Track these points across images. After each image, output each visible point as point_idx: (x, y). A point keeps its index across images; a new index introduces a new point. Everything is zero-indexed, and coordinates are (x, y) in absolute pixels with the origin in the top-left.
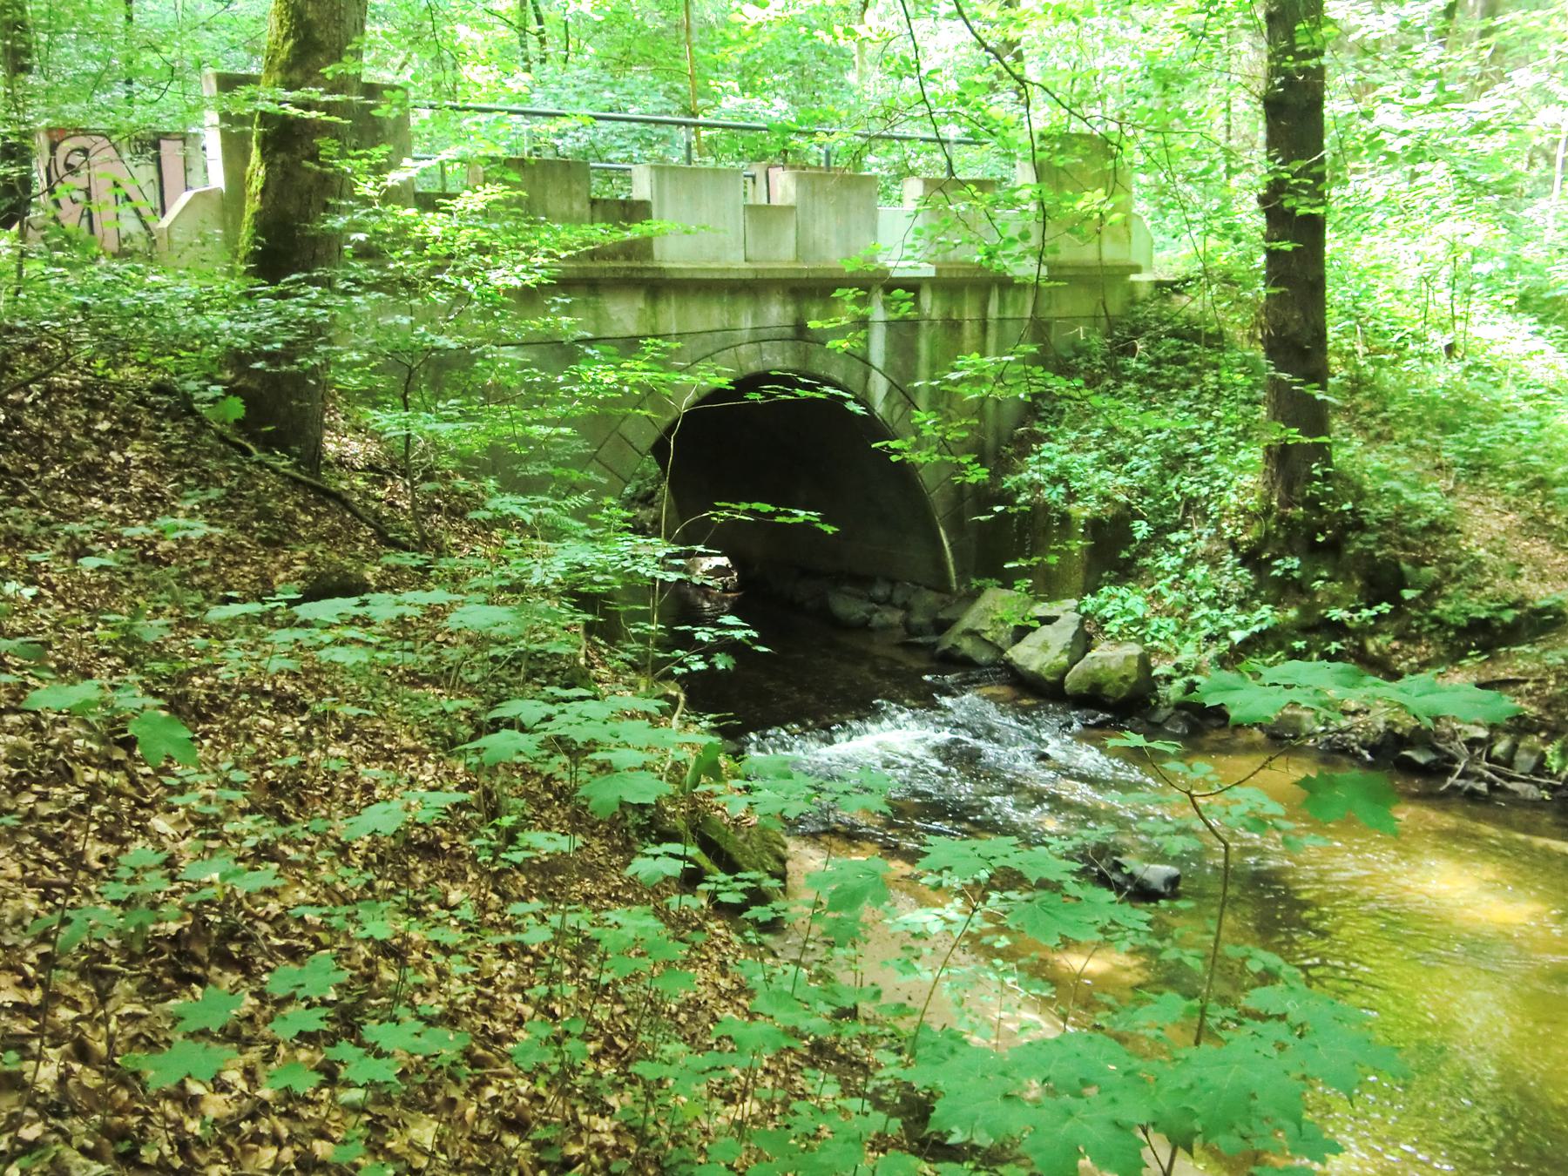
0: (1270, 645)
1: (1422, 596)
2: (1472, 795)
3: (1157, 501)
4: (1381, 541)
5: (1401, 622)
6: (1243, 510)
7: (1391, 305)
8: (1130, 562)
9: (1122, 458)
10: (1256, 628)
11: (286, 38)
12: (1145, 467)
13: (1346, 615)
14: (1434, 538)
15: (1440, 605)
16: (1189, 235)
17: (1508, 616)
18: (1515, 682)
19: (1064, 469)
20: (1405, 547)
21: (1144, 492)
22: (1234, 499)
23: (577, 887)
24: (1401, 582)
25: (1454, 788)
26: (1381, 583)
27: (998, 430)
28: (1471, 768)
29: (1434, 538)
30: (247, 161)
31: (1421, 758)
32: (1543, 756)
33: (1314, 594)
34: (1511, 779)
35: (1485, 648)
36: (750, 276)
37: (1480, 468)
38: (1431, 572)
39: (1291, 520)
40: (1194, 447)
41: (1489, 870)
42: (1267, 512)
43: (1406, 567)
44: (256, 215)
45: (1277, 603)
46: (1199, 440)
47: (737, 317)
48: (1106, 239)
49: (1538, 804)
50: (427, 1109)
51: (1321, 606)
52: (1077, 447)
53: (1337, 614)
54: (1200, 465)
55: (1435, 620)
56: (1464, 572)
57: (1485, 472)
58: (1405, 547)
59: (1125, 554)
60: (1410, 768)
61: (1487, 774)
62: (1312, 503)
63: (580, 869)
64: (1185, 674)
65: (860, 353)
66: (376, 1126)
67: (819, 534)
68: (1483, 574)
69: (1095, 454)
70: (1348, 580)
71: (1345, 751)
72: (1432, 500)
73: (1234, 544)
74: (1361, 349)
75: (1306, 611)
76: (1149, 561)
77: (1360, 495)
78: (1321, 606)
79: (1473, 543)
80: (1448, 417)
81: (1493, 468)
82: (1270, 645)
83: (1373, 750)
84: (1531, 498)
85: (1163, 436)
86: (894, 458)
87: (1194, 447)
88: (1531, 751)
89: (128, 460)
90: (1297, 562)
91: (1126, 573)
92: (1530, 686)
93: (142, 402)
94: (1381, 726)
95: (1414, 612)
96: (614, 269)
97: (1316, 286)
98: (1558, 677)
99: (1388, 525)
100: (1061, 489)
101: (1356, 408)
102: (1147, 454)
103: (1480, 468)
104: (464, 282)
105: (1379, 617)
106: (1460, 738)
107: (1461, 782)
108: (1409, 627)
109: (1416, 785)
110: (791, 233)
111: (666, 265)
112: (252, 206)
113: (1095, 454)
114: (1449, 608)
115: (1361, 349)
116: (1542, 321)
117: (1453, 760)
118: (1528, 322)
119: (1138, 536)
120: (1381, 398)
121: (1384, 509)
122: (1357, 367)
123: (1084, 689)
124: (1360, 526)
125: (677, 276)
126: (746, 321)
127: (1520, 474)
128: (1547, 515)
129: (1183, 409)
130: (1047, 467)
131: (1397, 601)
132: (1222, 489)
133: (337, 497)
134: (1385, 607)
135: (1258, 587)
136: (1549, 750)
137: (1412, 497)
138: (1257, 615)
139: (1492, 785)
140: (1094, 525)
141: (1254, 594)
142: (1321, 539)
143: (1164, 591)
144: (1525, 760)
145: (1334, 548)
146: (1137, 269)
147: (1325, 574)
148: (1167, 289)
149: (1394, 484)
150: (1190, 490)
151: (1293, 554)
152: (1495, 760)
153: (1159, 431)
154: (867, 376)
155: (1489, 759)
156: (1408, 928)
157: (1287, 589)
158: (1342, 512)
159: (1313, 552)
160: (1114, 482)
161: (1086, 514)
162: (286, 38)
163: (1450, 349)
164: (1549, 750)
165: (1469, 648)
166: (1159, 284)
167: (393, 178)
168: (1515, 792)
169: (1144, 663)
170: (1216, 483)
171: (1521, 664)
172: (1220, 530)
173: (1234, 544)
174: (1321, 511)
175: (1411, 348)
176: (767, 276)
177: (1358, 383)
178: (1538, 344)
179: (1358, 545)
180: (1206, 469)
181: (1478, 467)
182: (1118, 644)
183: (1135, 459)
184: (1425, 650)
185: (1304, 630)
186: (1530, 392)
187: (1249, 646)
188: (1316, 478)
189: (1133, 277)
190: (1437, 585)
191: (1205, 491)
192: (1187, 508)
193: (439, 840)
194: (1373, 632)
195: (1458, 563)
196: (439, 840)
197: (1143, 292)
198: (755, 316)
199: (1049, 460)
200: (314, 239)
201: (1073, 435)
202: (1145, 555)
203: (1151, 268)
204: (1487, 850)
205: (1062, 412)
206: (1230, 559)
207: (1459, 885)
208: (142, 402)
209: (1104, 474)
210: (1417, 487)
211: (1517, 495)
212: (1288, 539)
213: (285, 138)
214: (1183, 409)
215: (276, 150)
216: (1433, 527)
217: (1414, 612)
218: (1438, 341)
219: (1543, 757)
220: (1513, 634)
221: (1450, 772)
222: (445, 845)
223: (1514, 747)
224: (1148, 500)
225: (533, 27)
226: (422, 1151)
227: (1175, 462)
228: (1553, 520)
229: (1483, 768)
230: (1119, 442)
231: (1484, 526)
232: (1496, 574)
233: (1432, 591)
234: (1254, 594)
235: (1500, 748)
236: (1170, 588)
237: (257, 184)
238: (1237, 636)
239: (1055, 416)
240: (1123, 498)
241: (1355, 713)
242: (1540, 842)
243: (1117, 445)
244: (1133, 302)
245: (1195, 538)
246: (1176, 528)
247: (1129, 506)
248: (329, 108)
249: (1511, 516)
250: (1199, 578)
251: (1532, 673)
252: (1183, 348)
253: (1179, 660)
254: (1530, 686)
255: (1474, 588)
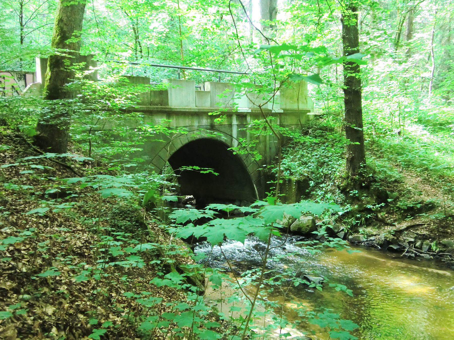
0: (350, 216)
1: (394, 201)
2: (410, 257)
3: (316, 175)
4: (381, 185)
5: (388, 209)
6: (341, 177)
7: (382, 121)
8: (309, 193)
9: (306, 163)
10: (346, 211)
11: (58, 35)
12: (313, 166)
13: (372, 207)
14: (396, 184)
15: (399, 203)
16: (323, 101)
17: (419, 206)
18: (422, 225)
19: (289, 166)
20: (388, 187)
21: (312, 173)
22: (338, 174)
23: (136, 280)
24: (387, 197)
25: (405, 256)
26: (381, 197)
27: (270, 157)
28: (409, 250)
29: (396, 184)
30: (46, 70)
31: (395, 247)
32: (431, 246)
33: (363, 201)
34: (421, 253)
35: (412, 215)
36: (197, 111)
37: (409, 165)
38: (396, 194)
39: (355, 179)
40: (326, 160)
41: (416, 277)
42: (348, 177)
43: (389, 193)
44: (48, 86)
45: (351, 204)
46: (328, 157)
47: (193, 122)
48: (300, 102)
49: (430, 260)
50: (51, 304)
51: (364, 204)
52: (293, 160)
53: (369, 206)
54: (328, 165)
55: (398, 207)
56: (405, 194)
57: (411, 166)
58: (388, 187)
59: (307, 191)
60: (392, 250)
61: (414, 251)
62: (360, 174)
63: (137, 275)
64: (326, 225)
65: (229, 134)
66: (31, 306)
67: (212, 172)
68: (411, 194)
69: (298, 162)
70: (372, 197)
71: (373, 246)
72: (395, 174)
73: (339, 187)
74: (374, 133)
75: (360, 206)
76: (314, 192)
77: (375, 172)
78: (364, 204)
79: (408, 186)
80: (400, 151)
81: (412, 165)
82: (350, 216)
83: (381, 245)
84: (424, 173)
85: (317, 157)
86: (234, 153)
87: (326, 160)
88: (427, 245)
89: (6, 155)
90: (357, 192)
91: (308, 196)
92: (426, 226)
93: (12, 140)
94: (383, 239)
95: (392, 205)
96: (157, 108)
97: (359, 113)
98: (434, 223)
99: (383, 181)
100: (288, 172)
101: (373, 149)
102: (313, 162)
103: (409, 165)
104: (107, 102)
105: (381, 207)
106: (406, 241)
107: (407, 254)
108: (390, 210)
109: (394, 255)
110: (209, 99)
111: (172, 107)
112: (47, 84)
113: (298, 162)
114: (402, 204)
115: (374, 133)
116: (426, 126)
117: (404, 248)
118: (421, 127)
119: (311, 185)
120: (380, 146)
121: (381, 176)
122: (373, 138)
123: (296, 229)
124: (375, 181)
125: (176, 110)
126: (196, 124)
127: (420, 166)
128: (429, 178)
129: (323, 149)
130: (284, 166)
131: (386, 202)
132: (335, 171)
133: (69, 168)
134: (383, 204)
135: (346, 200)
136: (432, 244)
137: (389, 173)
138: (346, 207)
139: (416, 254)
140: (298, 182)
141: (345, 201)
142: (364, 185)
143: (319, 201)
144: (425, 247)
145: (367, 188)
146: (309, 111)
147: (365, 195)
148: (318, 117)
149: (385, 169)
150: (325, 172)
151: (356, 189)
152: (417, 248)
153: (316, 155)
154: (232, 140)
155: (415, 247)
156: (392, 294)
157: (355, 200)
158: (369, 177)
159: (361, 188)
160: (304, 170)
161: (296, 179)
162: (58, 35)
163: (399, 133)
164: (432, 244)
165: (408, 215)
166: (316, 116)
167: (87, 73)
168: (423, 257)
169: (314, 221)
170: (333, 170)
171: (423, 220)
172: (335, 183)
173: (339, 187)
174: (363, 177)
175: (388, 133)
176: (202, 111)
177: (373, 142)
178: (425, 132)
179: (374, 186)
180: (330, 166)
181: (408, 165)
182: (306, 216)
183: (309, 163)
184: (395, 217)
185: (360, 211)
186: (423, 144)
187: (344, 216)
188: (361, 167)
189: (308, 114)
190: (398, 198)
191: (330, 172)
192: (325, 177)
193: (85, 253)
194: (380, 212)
195: (404, 191)
196: (85, 253)
197: (311, 118)
198: (199, 123)
199: (285, 164)
200: (65, 93)
201: (292, 157)
202: (313, 191)
203: (313, 111)
204: (414, 272)
205: (288, 151)
206: (338, 191)
207: (408, 283)
208: (12, 140)
209: (300, 168)
210: (391, 170)
211: (420, 172)
212: (354, 185)
213: (56, 63)
214: (323, 149)
215: (54, 67)
216: (396, 181)
217: (392, 205)
218: (397, 131)
219: (430, 246)
220: (420, 211)
221: (404, 251)
222: (86, 254)
223: (422, 244)
224: (313, 175)
225: (139, 48)
226: (47, 315)
227: (322, 164)
228: (431, 179)
229: (413, 250)
230: (305, 159)
231: (411, 181)
232: (415, 194)
233: (396, 200)
234: (345, 201)
235: (418, 244)
236: (321, 200)
237: (48, 77)
238: (340, 213)
239: (286, 152)
240: (306, 174)
241: (375, 235)
242: (430, 270)
243: (305, 159)
244: (308, 120)
245: (328, 185)
246: (322, 183)
247: (308, 177)
248: (70, 53)
249: (419, 179)
250: (329, 197)
251: (426, 222)
252: (322, 133)
253: (324, 221)
254: (426, 226)
255: (408, 198)
